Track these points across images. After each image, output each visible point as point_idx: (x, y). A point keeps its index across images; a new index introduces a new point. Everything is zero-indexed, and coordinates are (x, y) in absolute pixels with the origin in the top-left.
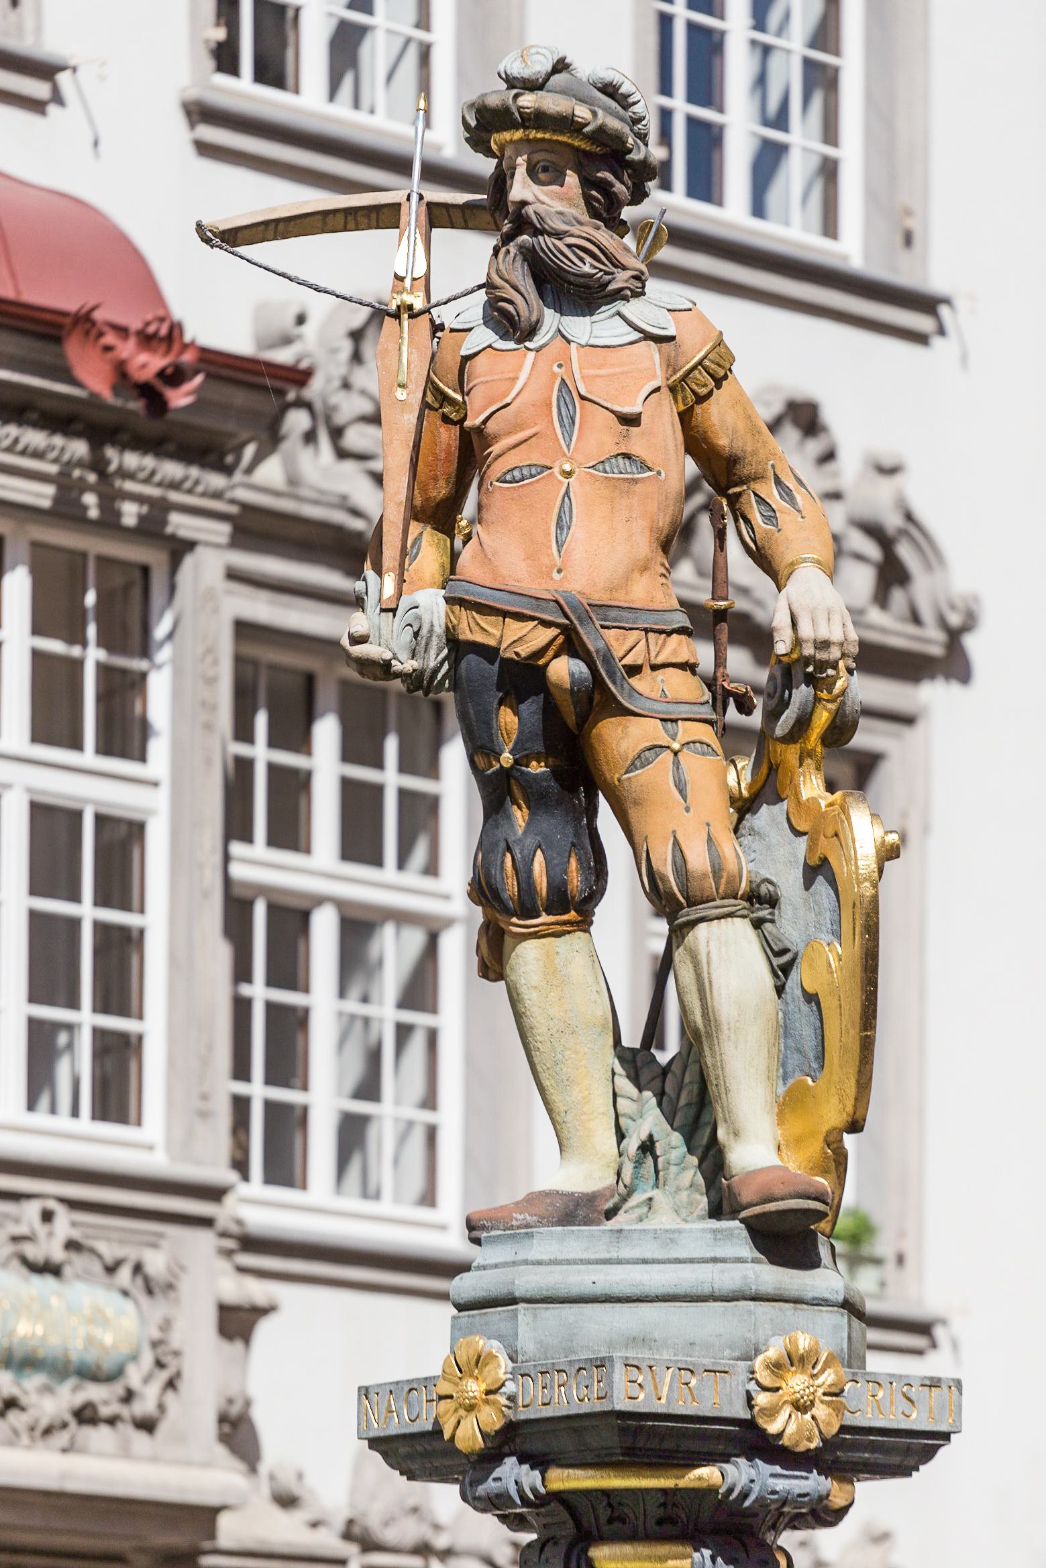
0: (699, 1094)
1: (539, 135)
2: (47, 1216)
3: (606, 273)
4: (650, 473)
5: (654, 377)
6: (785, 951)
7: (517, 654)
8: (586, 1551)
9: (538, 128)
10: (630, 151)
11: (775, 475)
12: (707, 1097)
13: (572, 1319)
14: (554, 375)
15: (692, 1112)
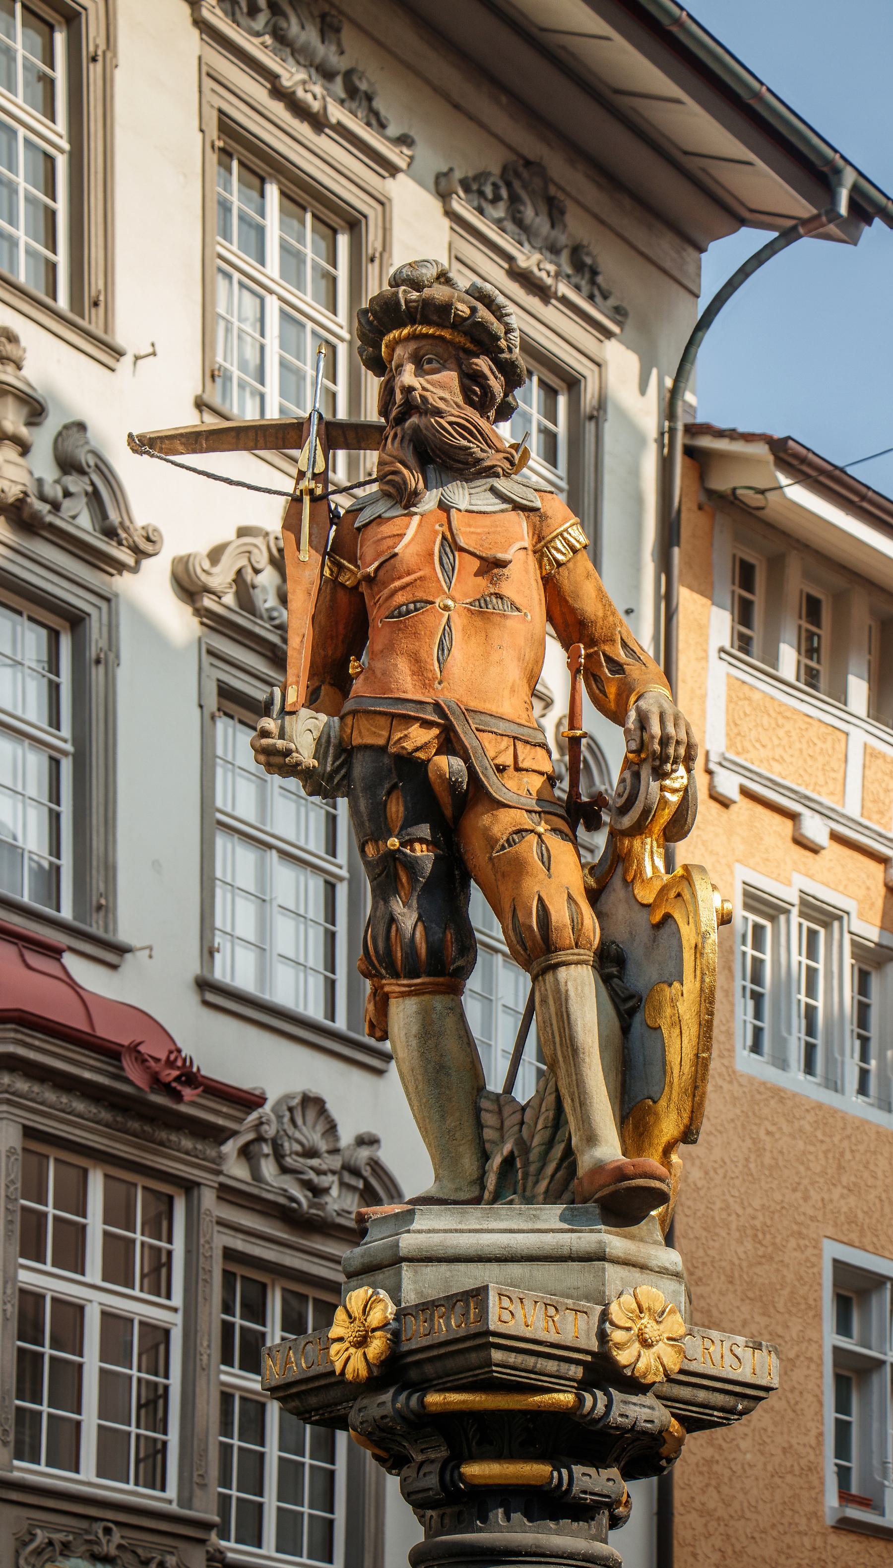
0: (554, 1119)
1: (424, 330)
2: (107, 1531)
3: (482, 450)
4: (516, 613)
5: (523, 539)
6: (631, 997)
7: (403, 748)
8: (459, 1467)
9: (426, 322)
10: (502, 351)
11: (622, 639)
12: (563, 1116)
13: (448, 1274)
14: (436, 532)
15: (548, 1132)
